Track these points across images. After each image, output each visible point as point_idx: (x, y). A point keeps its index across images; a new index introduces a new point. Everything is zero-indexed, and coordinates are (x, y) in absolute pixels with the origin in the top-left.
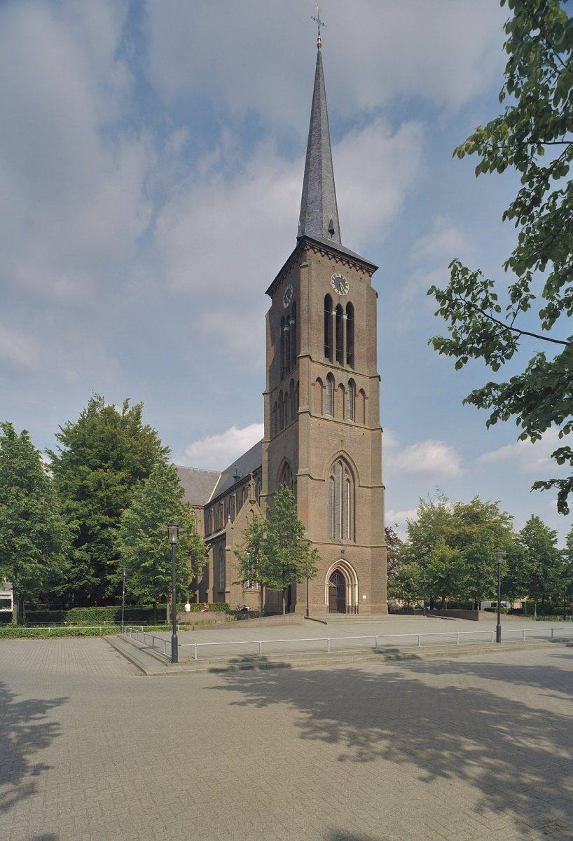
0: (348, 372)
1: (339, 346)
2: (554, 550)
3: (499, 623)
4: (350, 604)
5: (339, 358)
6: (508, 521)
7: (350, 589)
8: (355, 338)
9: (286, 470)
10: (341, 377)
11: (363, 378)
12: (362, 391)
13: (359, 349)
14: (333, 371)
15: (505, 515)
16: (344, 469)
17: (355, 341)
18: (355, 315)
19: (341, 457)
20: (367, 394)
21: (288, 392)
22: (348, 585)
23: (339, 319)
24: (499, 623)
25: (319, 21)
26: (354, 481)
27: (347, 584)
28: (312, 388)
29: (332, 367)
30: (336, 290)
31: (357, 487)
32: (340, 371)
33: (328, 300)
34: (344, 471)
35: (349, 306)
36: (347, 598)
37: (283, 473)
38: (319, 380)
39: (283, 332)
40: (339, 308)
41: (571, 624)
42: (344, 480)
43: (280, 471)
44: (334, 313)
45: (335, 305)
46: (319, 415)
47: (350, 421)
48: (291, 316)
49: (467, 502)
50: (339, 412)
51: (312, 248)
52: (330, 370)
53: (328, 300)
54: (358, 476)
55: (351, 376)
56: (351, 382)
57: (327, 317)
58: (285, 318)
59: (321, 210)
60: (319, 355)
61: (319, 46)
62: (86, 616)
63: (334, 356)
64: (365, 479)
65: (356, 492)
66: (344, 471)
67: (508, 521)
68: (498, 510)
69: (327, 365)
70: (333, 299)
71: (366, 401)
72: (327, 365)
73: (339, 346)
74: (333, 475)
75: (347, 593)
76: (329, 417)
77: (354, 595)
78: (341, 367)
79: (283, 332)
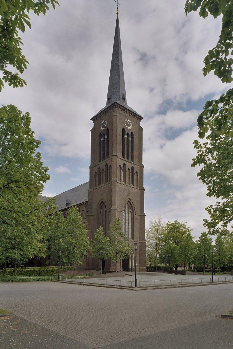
0: (131, 163)
1: (128, 151)
2: (211, 245)
3: (136, 278)
4: (131, 267)
5: (128, 158)
6: (190, 231)
7: (131, 261)
8: (134, 148)
9: (102, 204)
10: (129, 165)
11: (137, 166)
12: (137, 172)
13: (135, 153)
14: (126, 163)
15: (189, 228)
16: (129, 207)
17: (134, 149)
18: (134, 138)
19: (129, 201)
20: (139, 174)
21: (104, 169)
22: (130, 259)
23: (128, 138)
24: (136, 278)
25: (117, 3)
26: (133, 212)
27: (129, 258)
28: (117, 169)
29: (125, 161)
30: (127, 127)
31: (134, 215)
32: (128, 163)
33: (124, 130)
34: (129, 208)
35: (132, 133)
36: (129, 265)
37: (100, 206)
38: (120, 166)
39: (100, 141)
40: (128, 134)
41: (232, 276)
42: (129, 212)
43: (99, 205)
44: (126, 136)
45: (126, 133)
46: (120, 182)
47: (131, 185)
48: (105, 134)
49: (172, 222)
50: (127, 181)
51: (118, 107)
52: (124, 162)
53: (124, 130)
54: (135, 211)
55: (133, 165)
56: (133, 168)
57: (123, 137)
58: (102, 134)
59: (120, 88)
60: (120, 155)
61: (117, 11)
62: (11, 273)
63: (126, 156)
64: (137, 212)
65: (134, 217)
66: (129, 208)
67: (190, 231)
68: (186, 226)
69: (123, 160)
70: (126, 130)
71: (138, 177)
72: (123, 160)
73: (128, 151)
74: (125, 209)
75: (129, 262)
76: (123, 183)
77: (132, 264)
78: (128, 161)
79: (100, 141)
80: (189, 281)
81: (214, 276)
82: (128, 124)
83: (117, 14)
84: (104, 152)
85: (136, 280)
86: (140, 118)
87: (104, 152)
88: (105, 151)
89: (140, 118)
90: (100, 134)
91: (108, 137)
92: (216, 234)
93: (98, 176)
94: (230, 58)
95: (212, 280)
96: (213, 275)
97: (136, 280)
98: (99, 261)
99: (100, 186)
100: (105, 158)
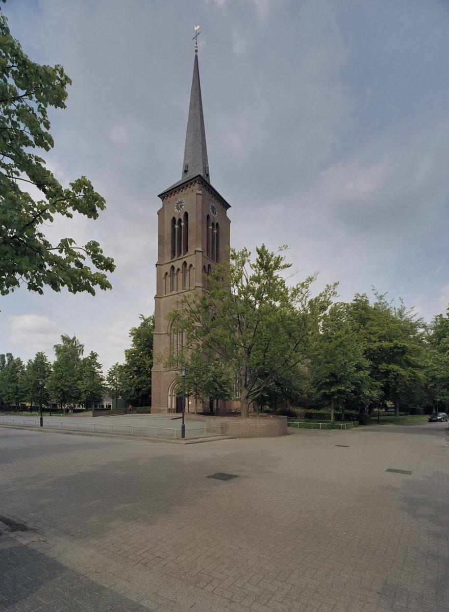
3: (183, 423)
23: (213, 230)
80: (22, 423)
81: (44, 418)
82: (213, 211)
83: (196, 51)
84: (180, 244)
85: (183, 427)
86: (227, 206)
87: (180, 244)
88: (216, 242)
89: (227, 206)
90: (174, 219)
91: (207, 227)
92: (384, 393)
93: (182, 274)
94: (51, 141)
95: (42, 425)
96: (41, 416)
97: (183, 427)
98: (354, 409)
99: (172, 293)
100: (182, 252)
